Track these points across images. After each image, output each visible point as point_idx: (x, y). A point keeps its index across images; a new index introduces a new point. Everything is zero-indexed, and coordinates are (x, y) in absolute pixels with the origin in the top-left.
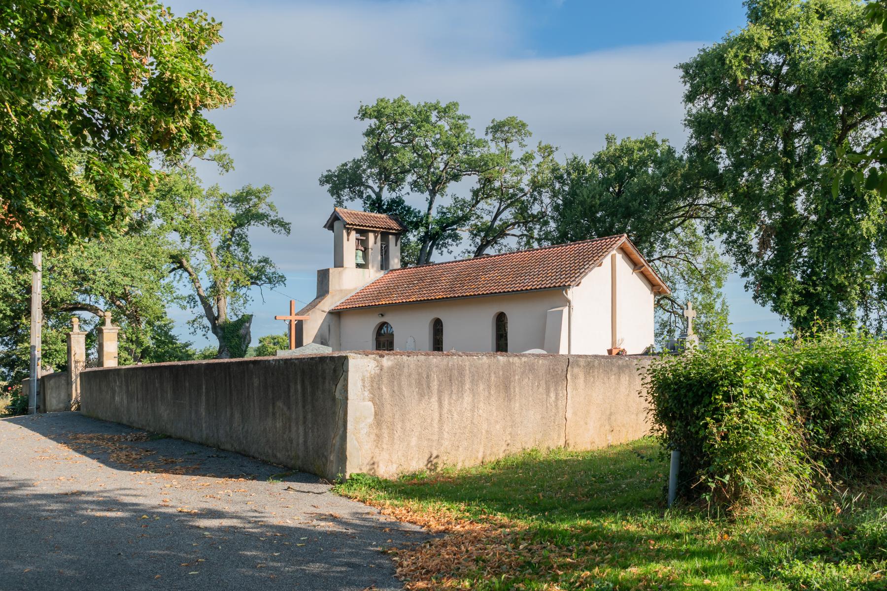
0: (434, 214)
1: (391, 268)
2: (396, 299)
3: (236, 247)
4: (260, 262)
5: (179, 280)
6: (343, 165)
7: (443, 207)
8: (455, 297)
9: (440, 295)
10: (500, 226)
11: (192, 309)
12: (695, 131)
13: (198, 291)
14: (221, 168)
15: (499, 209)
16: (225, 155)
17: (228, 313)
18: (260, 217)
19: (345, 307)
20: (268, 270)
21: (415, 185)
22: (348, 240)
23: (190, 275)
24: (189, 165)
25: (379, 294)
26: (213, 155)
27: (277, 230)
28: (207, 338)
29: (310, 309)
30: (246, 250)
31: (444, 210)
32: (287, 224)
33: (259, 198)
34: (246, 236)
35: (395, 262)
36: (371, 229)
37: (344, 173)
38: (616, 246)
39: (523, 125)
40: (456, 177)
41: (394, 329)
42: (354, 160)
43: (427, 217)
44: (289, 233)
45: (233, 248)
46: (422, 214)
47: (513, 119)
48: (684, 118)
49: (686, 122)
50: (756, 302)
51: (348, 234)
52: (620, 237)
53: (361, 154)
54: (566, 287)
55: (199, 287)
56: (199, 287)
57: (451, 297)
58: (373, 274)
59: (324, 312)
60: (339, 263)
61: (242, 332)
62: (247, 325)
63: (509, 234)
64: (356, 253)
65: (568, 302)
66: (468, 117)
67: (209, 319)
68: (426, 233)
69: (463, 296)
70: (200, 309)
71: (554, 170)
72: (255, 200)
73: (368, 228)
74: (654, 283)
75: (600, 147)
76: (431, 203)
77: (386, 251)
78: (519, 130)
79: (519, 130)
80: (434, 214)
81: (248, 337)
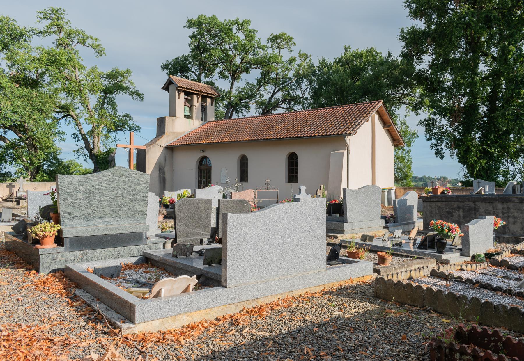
0: (234, 91)
1: (208, 120)
2: (214, 140)
3: (108, 106)
4: (123, 116)
5: (69, 124)
6: (176, 59)
7: (239, 88)
8: (258, 139)
9: (247, 138)
10: (274, 102)
11: (76, 143)
12: (406, 44)
13: (80, 131)
14: (97, 54)
15: (274, 91)
16: (99, 45)
17: (101, 147)
18: (124, 89)
19: (176, 144)
20: (129, 122)
21: (221, 74)
22: (179, 98)
23: (75, 120)
24: (74, 48)
25: (201, 136)
26: (91, 43)
27: (135, 98)
28: (87, 162)
29: (151, 144)
30: (114, 109)
31: (240, 90)
32: (141, 94)
33: (124, 77)
34: (115, 99)
35: (211, 117)
36: (195, 92)
37: (177, 63)
38: (375, 111)
39: (291, 39)
40: (247, 71)
41: (212, 161)
42: (183, 56)
43: (230, 93)
44: (142, 100)
45: (106, 106)
46: (227, 90)
47: (284, 34)
48: (400, 34)
49: (400, 37)
50: (437, 157)
51: (179, 94)
52: (378, 102)
53: (187, 51)
54: (347, 135)
55: (81, 129)
56: (81, 129)
57: (255, 140)
58: (195, 124)
59: (162, 147)
60: (172, 114)
61: (109, 159)
62: (113, 155)
63: (280, 107)
64: (185, 108)
65: (346, 146)
66: (256, 31)
67: (88, 150)
68: (229, 103)
69: (264, 139)
70: (82, 143)
71: (311, 67)
72: (121, 78)
73: (193, 91)
74: (395, 138)
75: (340, 53)
76: (232, 85)
77: (205, 109)
78: (287, 42)
79: (287, 42)
80: (234, 91)
81: (113, 163)
